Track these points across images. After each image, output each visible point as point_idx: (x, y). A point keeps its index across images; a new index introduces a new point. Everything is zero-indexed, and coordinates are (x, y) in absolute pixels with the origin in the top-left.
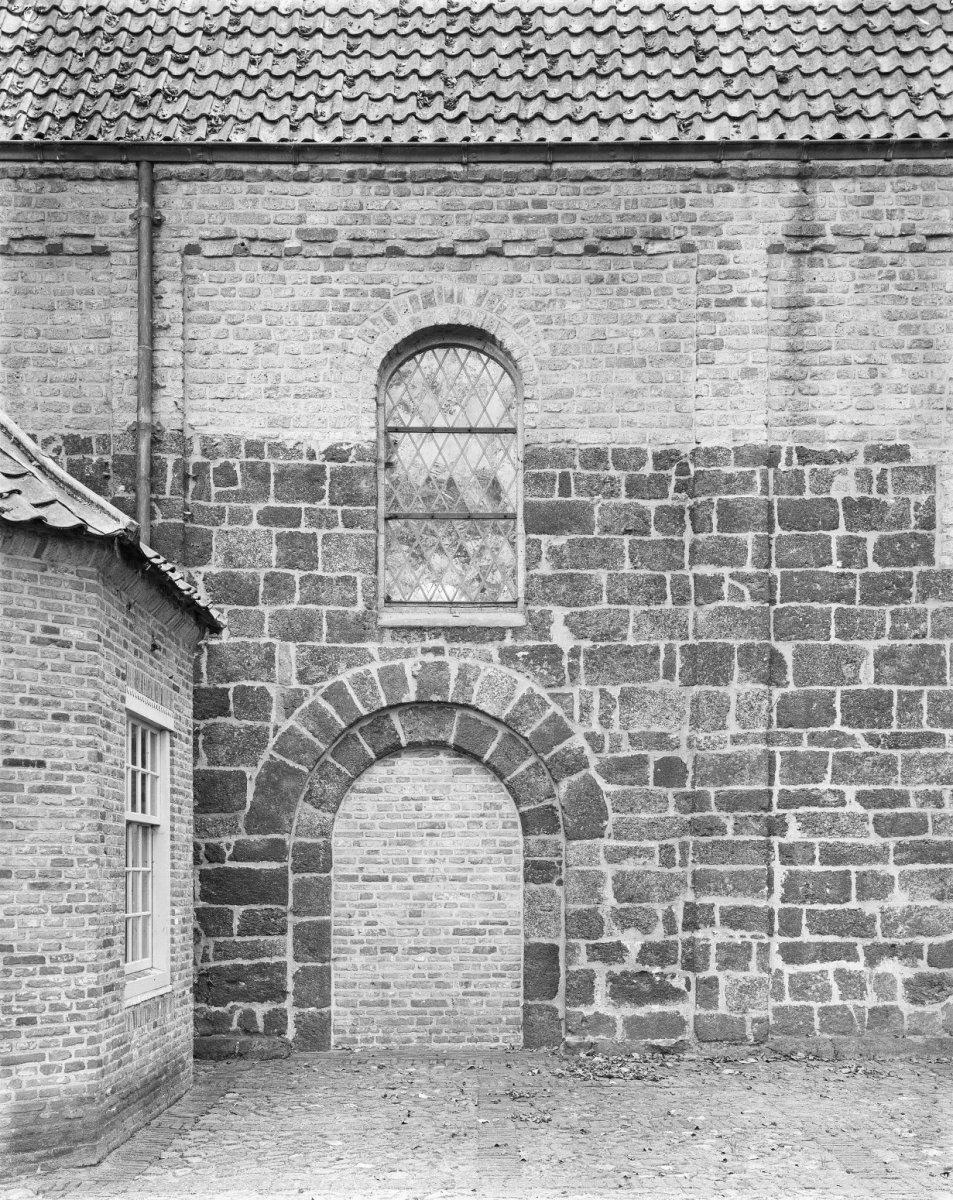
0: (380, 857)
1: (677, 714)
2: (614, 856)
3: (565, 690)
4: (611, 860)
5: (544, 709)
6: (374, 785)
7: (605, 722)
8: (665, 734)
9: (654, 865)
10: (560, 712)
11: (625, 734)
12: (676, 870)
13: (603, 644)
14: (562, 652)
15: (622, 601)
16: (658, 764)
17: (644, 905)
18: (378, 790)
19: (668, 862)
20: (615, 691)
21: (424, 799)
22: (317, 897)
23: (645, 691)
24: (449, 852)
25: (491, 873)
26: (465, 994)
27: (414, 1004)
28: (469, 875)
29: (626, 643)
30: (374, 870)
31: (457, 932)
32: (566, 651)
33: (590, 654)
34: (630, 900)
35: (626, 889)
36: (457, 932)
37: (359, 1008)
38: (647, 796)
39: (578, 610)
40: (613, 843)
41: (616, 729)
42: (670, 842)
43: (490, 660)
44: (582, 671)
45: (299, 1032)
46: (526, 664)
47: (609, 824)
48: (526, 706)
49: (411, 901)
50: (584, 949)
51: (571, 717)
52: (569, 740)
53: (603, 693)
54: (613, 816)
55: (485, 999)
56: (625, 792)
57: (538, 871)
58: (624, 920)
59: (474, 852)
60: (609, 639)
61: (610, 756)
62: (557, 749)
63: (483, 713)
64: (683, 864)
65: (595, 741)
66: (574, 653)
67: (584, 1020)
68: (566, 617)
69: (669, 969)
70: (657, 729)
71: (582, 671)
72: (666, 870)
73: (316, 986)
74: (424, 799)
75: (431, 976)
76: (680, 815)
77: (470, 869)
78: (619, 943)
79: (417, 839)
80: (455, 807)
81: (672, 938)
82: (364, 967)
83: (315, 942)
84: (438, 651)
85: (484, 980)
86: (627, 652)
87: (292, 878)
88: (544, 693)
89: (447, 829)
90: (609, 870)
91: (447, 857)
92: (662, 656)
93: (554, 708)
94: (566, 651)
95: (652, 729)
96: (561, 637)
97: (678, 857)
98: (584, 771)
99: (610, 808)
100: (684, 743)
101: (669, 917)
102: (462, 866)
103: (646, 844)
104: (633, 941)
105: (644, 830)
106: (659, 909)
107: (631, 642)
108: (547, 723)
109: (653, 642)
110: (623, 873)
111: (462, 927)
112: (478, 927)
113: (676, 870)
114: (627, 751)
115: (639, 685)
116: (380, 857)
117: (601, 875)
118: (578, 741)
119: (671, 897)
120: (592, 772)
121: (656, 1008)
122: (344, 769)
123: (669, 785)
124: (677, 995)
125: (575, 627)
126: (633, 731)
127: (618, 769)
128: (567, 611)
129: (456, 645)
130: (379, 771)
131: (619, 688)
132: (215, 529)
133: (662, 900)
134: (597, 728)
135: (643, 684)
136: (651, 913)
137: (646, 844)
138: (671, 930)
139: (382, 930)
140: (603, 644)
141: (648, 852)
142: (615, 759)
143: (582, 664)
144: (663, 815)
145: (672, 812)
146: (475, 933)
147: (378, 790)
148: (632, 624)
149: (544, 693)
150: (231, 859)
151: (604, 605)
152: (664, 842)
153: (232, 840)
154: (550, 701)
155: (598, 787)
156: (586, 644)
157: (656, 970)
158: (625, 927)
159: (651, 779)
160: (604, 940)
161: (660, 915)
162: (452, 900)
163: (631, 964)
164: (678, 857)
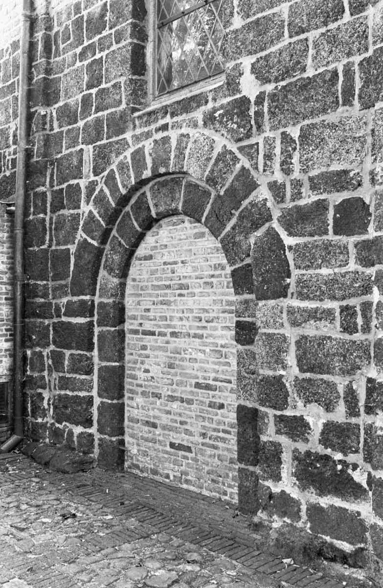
0: (151, 314)
1: (358, 145)
2: (297, 318)
3: (252, 141)
4: (295, 324)
5: (234, 164)
6: (149, 252)
7: (286, 169)
8: (346, 172)
9: (333, 330)
10: (247, 165)
11: (304, 178)
12: (358, 337)
13: (283, 83)
14: (249, 101)
15: (303, 31)
16: (338, 208)
17: (325, 377)
18: (150, 257)
19: (349, 328)
20: (295, 132)
21: (175, 263)
22: (117, 345)
23: (323, 124)
24: (191, 311)
25: (219, 332)
26: (203, 444)
27: (172, 445)
28: (205, 332)
29: (305, 75)
30: (148, 326)
31: (198, 385)
32: (253, 99)
33: (273, 97)
34: (311, 370)
35: (312, 357)
36: (198, 385)
37: (141, 442)
38: (327, 247)
39: (263, 54)
40: (296, 303)
41: (296, 175)
42: (352, 302)
43: (196, 125)
44: (267, 116)
45: (101, 454)
46: (221, 122)
47: (291, 281)
48: (221, 165)
49: (169, 354)
50: (272, 419)
51: (257, 168)
52: (254, 194)
53: (284, 135)
54: (295, 273)
55: (217, 452)
56: (305, 245)
57: (245, 332)
58: (310, 392)
59: (207, 311)
60: (290, 76)
61: (291, 205)
62: (245, 203)
63: (173, 173)
64: (366, 329)
65: (277, 189)
66: (260, 99)
67: (271, 496)
68: (253, 65)
69: (352, 458)
70: (336, 167)
71: (267, 116)
72: (347, 337)
73: (115, 418)
74: (175, 263)
75: (182, 423)
76: (360, 268)
77: (205, 327)
78: (301, 418)
79: (172, 299)
80: (195, 269)
81: (354, 420)
82: (143, 408)
83: (115, 383)
84: (165, 127)
85: (215, 434)
86: (307, 85)
87: (97, 330)
88: (233, 147)
89: (190, 290)
90: (291, 334)
91: (191, 315)
92: (341, 79)
93: (244, 162)
94: (253, 99)
95: (331, 169)
96: (250, 87)
97: (360, 321)
98: (267, 225)
99: (291, 263)
100: (366, 180)
101: (351, 394)
102: (200, 324)
103: (328, 304)
104: (316, 418)
105: (324, 287)
106: (341, 383)
107: (310, 73)
108: (237, 178)
109: (331, 67)
110: (305, 338)
111: (201, 381)
112: (211, 382)
113: (358, 337)
114: (308, 198)
115: (317, 120)
116: (151, 314)
117: (284, 339)
118: (263, 193)
119: (353, 369)
120: (275, 225)
121: (338, 502)
122: (123, 242)
123: (350, 233)
124: (355, 491)
125: (261, 73)
126: (311, 174)
127: (297, 220)
128: (253, 59)
129: (62, 93)
130: (150, 239)
131: (298, 127)
132: (61, 75)
133: (344, 372)
134: (279, 177)
135: (322, 118)
136: (332, 386)
137: (328, 304)
138: (353, 411)
139: (152, 378)
140: (283, 83)
141: (328, 314)
142: (296, 207)
143: (266, 110)
144: (343, 270)
145: (353, 266)
146: (208, 387)
147: (150, 257)
148: (311, 52)
149: (233, 147)
150: (65, 315)
151: (286, 40)
152: (344, 303)
153: (65, 300)
154: (239, 156)
155: (280, 241)
156: (269, 88)
157: (338, 456)
158: (308, 401)
159: (330, 228)
160: (289, 413)
161: (341, 389)
162: (194, 356)
163: (314, 444)
164: (360, 321)
